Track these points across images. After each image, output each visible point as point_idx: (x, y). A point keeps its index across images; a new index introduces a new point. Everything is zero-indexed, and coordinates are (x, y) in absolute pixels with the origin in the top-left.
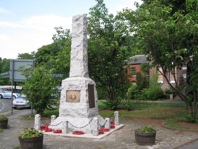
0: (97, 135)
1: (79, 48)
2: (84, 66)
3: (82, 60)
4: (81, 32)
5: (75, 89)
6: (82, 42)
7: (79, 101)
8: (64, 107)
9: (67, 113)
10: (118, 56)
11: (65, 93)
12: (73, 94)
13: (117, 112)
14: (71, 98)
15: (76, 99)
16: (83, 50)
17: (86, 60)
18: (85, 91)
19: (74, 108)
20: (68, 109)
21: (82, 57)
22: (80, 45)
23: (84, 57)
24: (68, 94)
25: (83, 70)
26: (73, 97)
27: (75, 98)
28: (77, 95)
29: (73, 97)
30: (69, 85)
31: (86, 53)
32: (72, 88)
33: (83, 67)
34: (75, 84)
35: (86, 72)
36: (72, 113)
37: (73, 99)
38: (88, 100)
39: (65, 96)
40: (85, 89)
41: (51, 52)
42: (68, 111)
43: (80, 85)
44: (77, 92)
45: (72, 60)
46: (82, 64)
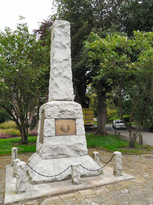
0: (142, 188)
4: (68, 43)
5: (69, 117)
7: (75, 133)
8: (55, 144)
9: (60, 152)
10: (137, 79)
11: (54, 123)
12: (64, 124)
14: (62, 129)
15: (71, 131)
19: (68, 144)
20: (61, 146)
22: (67, 60)
24: (57, 124)
26: (66, 128)
27: (69, 129)
29: (66, 128)
30: (59, 110)
32: (63, 115)
34: (69, 110)
36: (68, 151)
39: (54, 126)
41: (15, 44)
42: (61, 150)
43: (76, 111)
44: (71, 120)
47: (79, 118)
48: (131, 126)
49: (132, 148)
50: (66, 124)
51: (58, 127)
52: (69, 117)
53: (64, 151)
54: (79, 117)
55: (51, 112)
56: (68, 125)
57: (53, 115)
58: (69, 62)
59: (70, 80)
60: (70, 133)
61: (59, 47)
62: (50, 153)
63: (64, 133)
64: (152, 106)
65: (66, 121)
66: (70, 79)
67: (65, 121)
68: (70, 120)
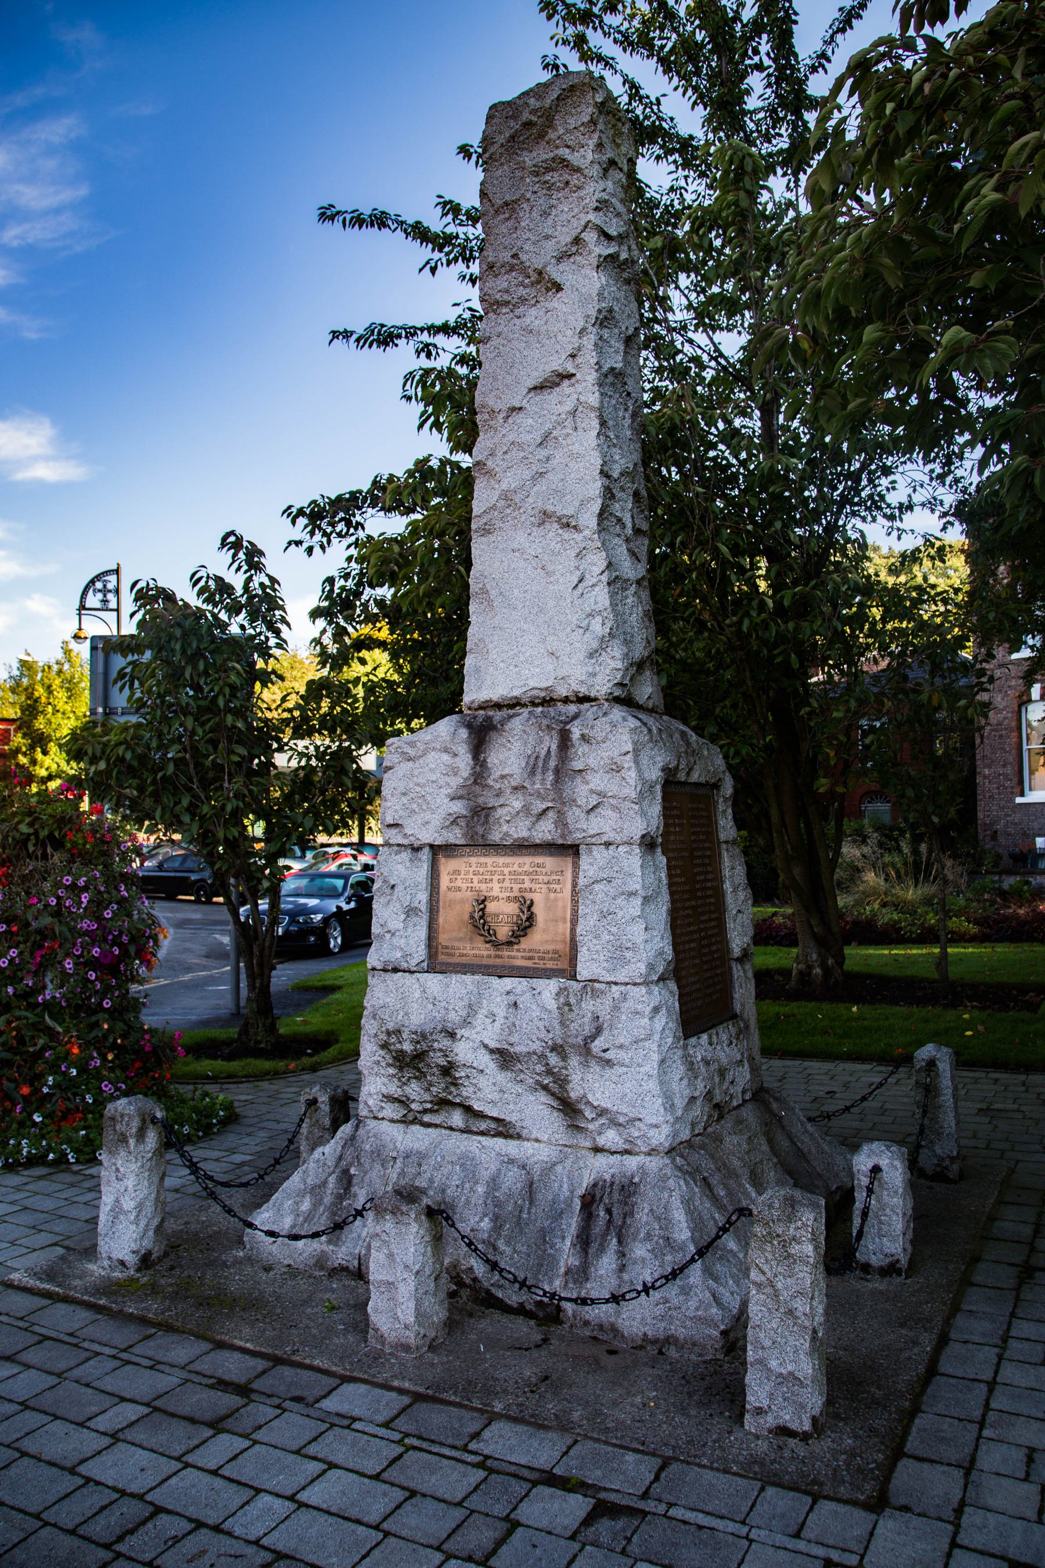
1: (565, 397)
2: (617, 584)
3: (593, 523)
4: (577, 241)
6: (589, 341)
13: (844, 850)
16: (603, 424)
17: (637, 531)
18: (637, 850)
21: (595, 487)
23: (608, 494)
24: (444, 882)
25: (598, 628)
28: (537, 897)
31: (623, 460)
33: (601, 597)
35: (639, 651)
37: (503, 932)
38: (669, 951)
40: (637, 828)
45: (486, 531)
46: (597, 562)
47: (605, 839)
48: (697, 785)
49: (230, 1139)
50: (507, 884)
51: (451, 904)
52: (525, 834)
53: (471, 1089)
54: (607, 829)
55: (404, 800)
56: (520, 890)
57: (419, 819)
58: (579, 388)
59: (578, 537)
60: (530, 958)
61: (507, 303)
62: (386, 1080)
63: (489, 956)
64: (742, 5)
65: (507, 865)
66: (575, 527)
67: (501, 860)
68: (540, 860)
